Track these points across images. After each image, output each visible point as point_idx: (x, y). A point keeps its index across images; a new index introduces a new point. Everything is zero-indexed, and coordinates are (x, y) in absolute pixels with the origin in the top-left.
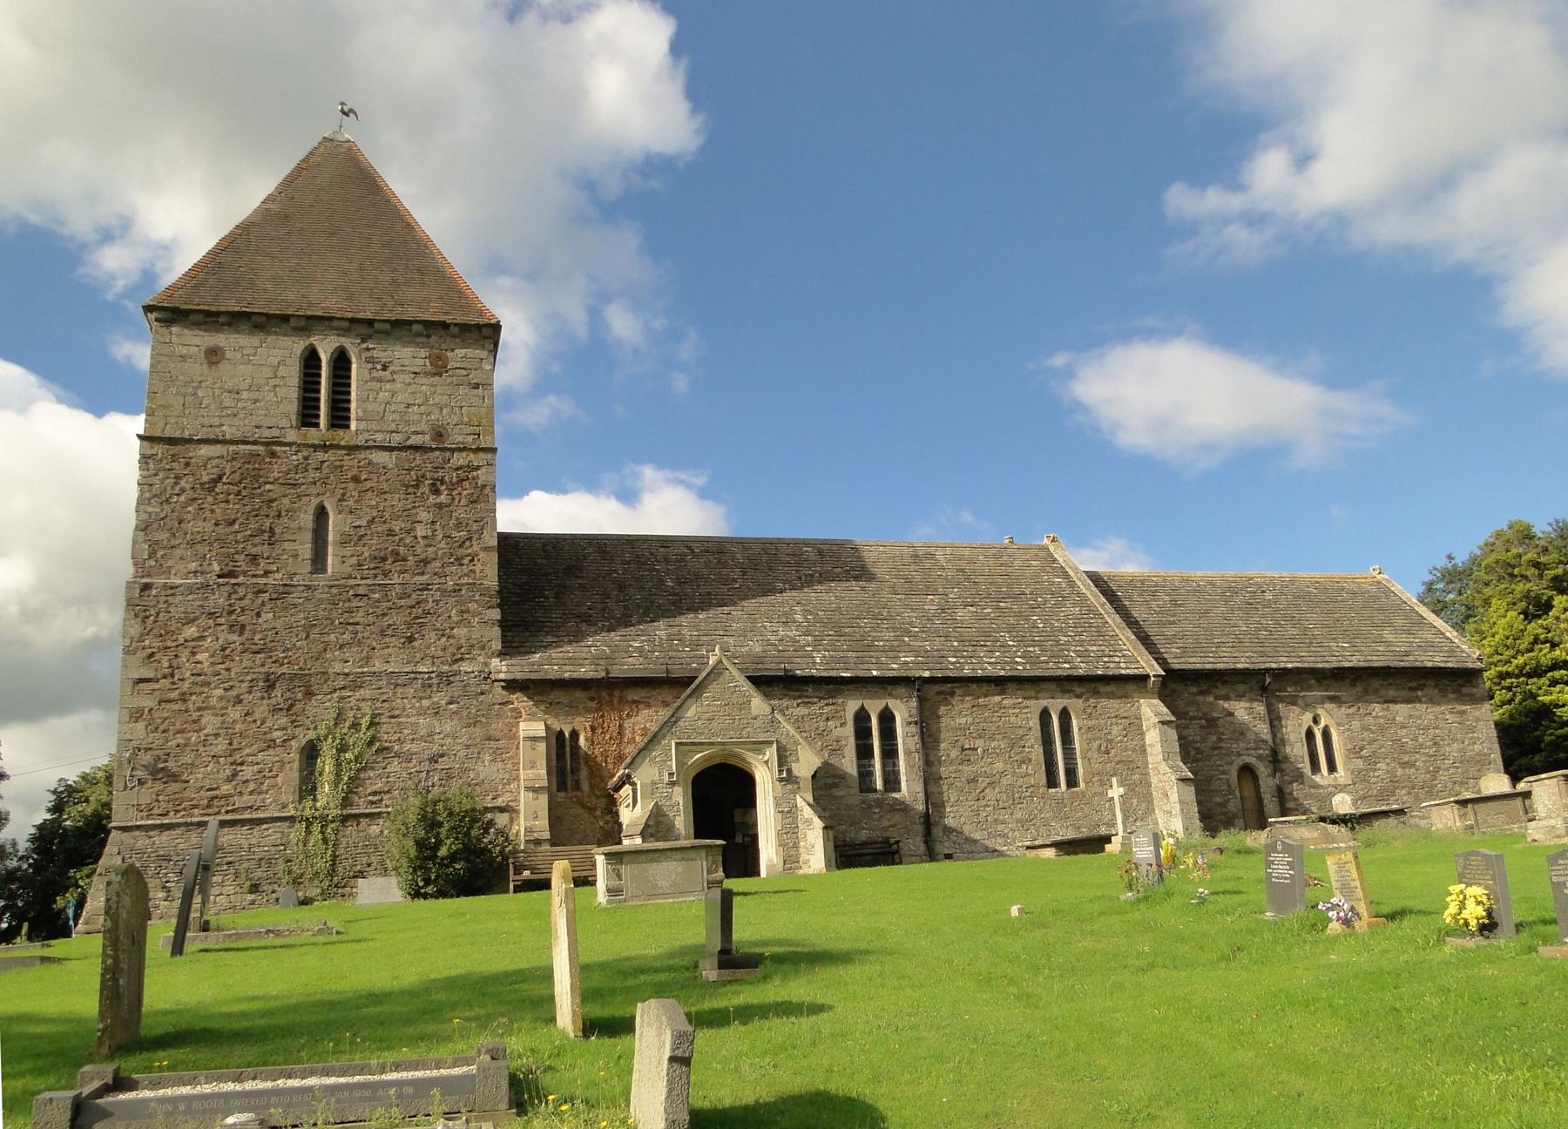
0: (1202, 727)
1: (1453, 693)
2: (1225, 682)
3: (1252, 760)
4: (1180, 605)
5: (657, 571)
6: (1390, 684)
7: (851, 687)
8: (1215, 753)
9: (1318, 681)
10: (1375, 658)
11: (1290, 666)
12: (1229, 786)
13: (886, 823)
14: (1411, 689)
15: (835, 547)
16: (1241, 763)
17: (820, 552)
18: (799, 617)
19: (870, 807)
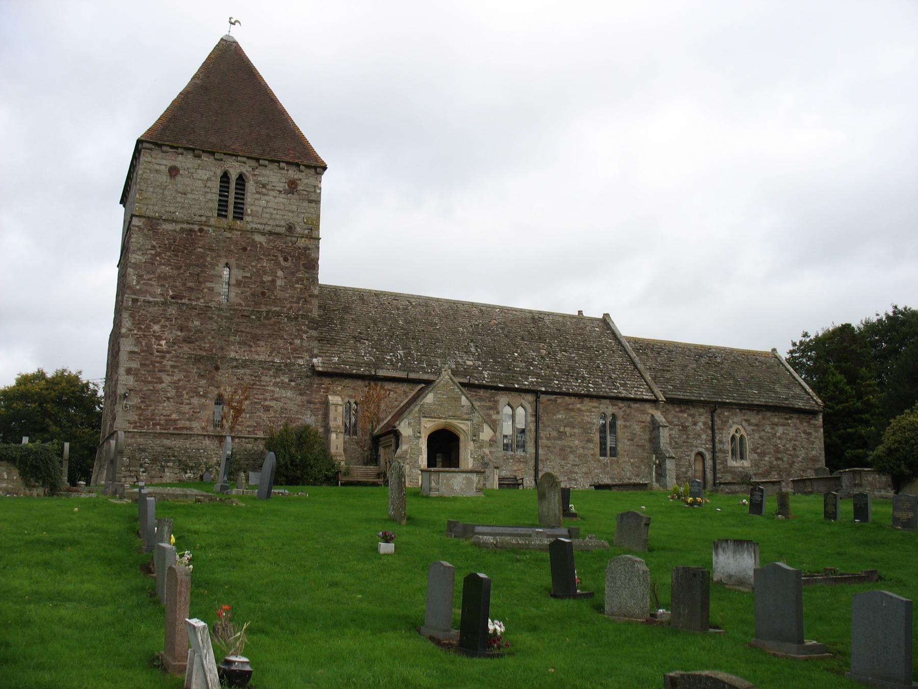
0: (679, 430)
1: (806, 422)
2: (694, 407)
3: (702, 450)
4: (673, 361)
5: (393, 314)
6: (776, 415)
7: (502, 392)
8: (685, 444)
9: (740, 410)
10: (770, 400)
11: (728, 401)
12: (690, 463)
13: (515, 468)
14: (786, 419)
15: (488, 309)
16: (697, 451)
17: (481, 310)
18: (473, 350)
19: (508, 459)
